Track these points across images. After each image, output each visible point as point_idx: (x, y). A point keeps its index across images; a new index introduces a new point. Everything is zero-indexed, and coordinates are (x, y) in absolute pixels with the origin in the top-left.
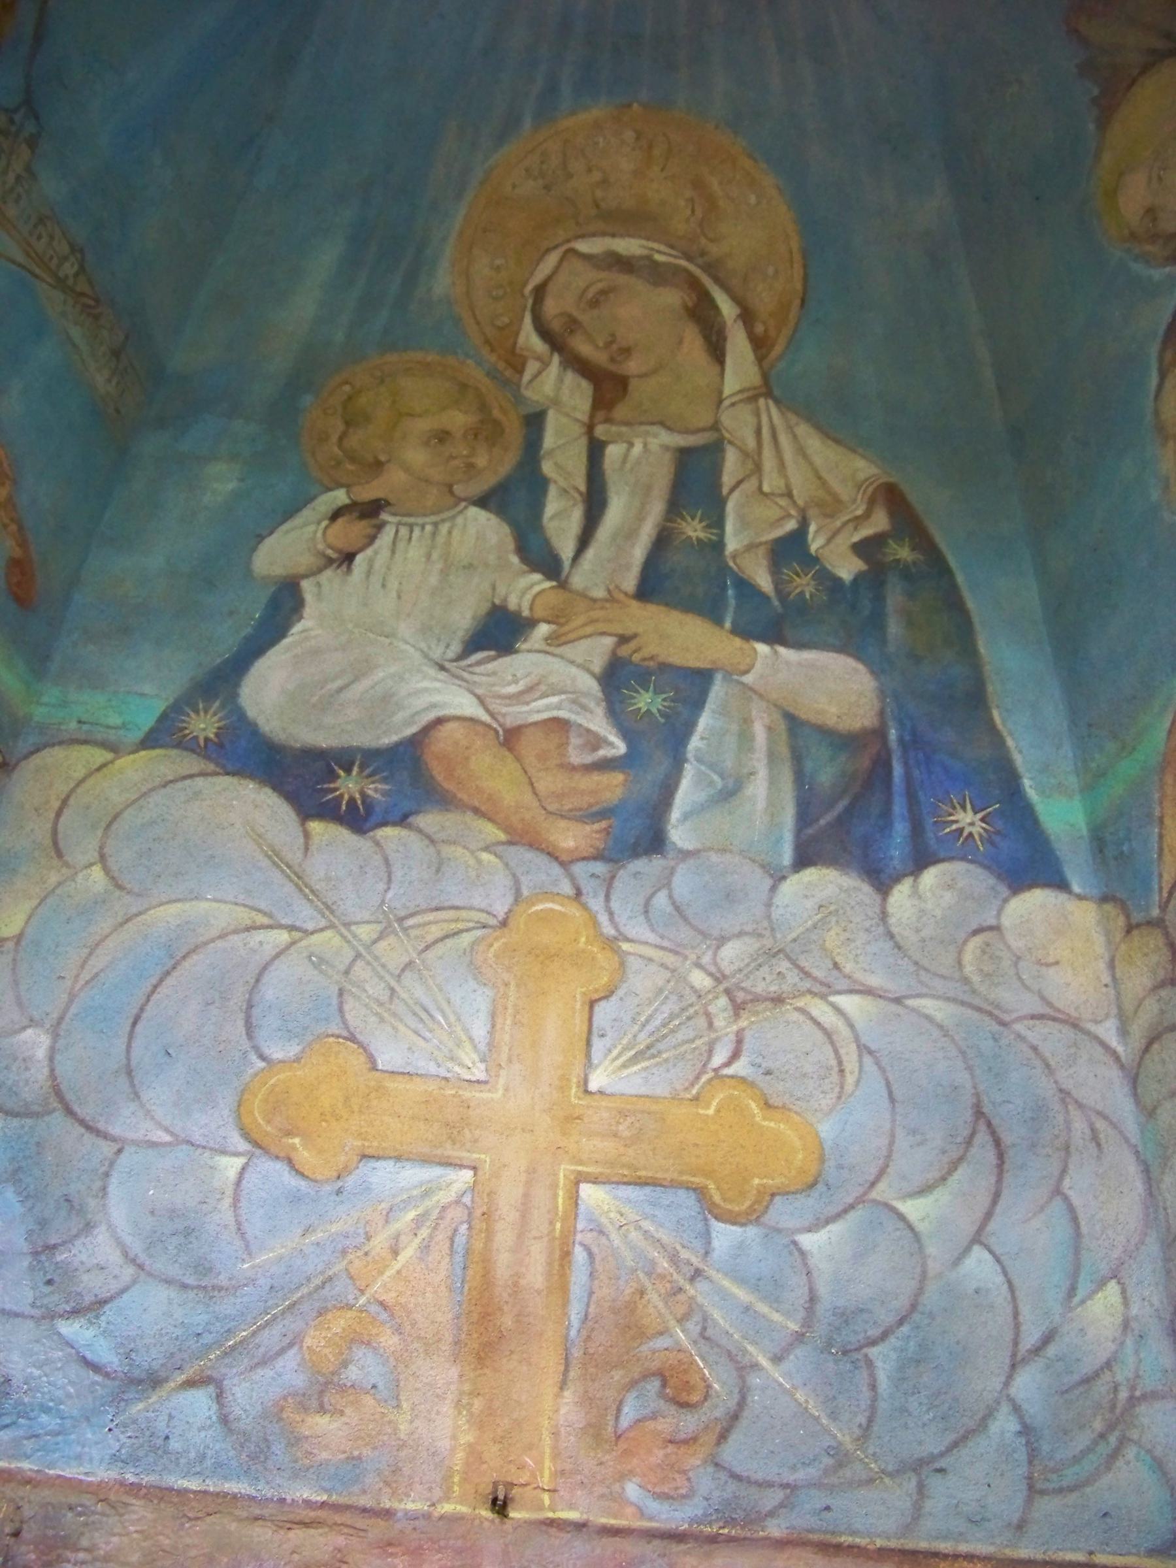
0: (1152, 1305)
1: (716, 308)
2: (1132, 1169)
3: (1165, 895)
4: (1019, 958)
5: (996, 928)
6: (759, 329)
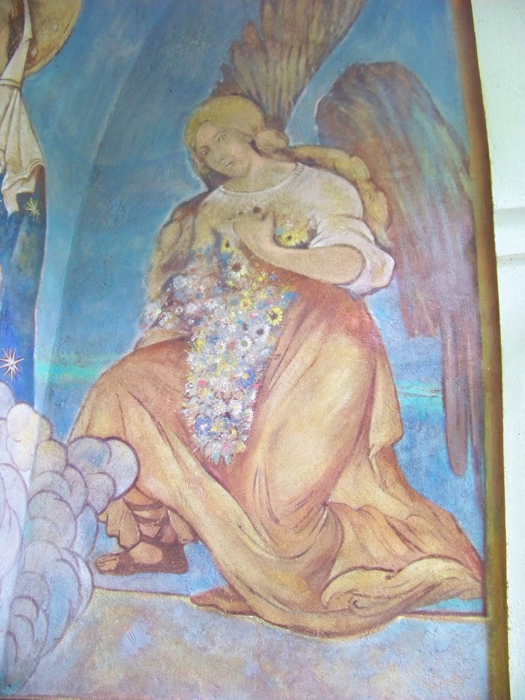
0: (8, 594)
1: (23, 27)
2: (18, 538)
3: (72, 438)
4: (9, 435)
5: (5, 419)
6: (34, 52)
